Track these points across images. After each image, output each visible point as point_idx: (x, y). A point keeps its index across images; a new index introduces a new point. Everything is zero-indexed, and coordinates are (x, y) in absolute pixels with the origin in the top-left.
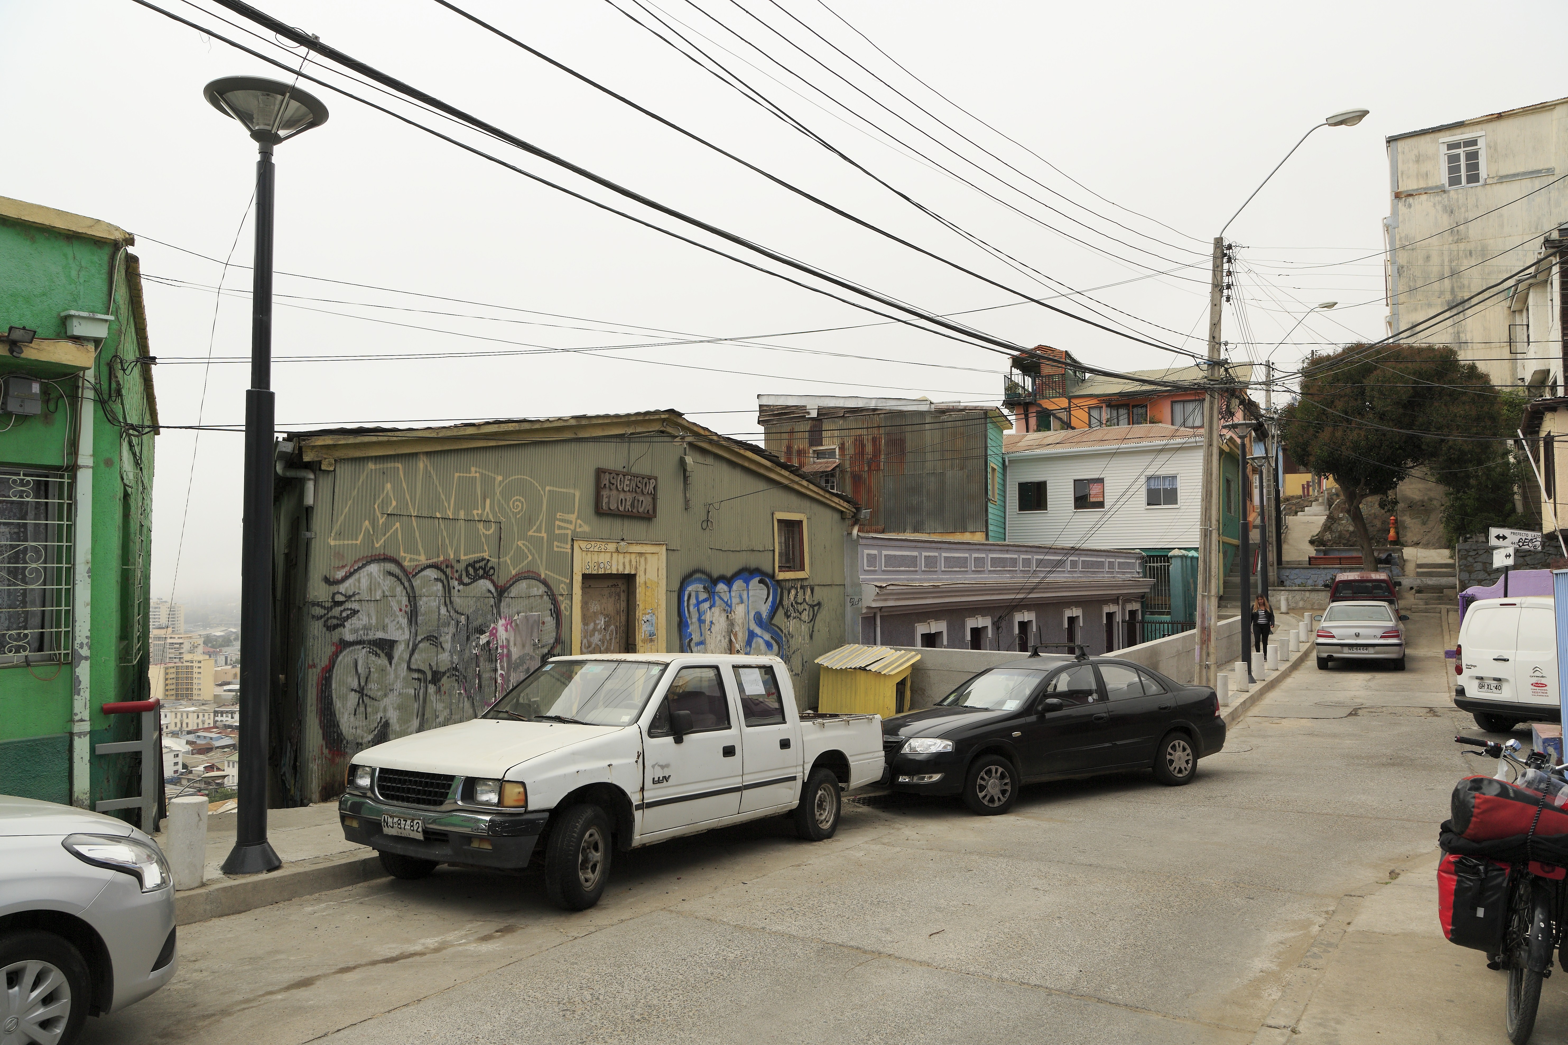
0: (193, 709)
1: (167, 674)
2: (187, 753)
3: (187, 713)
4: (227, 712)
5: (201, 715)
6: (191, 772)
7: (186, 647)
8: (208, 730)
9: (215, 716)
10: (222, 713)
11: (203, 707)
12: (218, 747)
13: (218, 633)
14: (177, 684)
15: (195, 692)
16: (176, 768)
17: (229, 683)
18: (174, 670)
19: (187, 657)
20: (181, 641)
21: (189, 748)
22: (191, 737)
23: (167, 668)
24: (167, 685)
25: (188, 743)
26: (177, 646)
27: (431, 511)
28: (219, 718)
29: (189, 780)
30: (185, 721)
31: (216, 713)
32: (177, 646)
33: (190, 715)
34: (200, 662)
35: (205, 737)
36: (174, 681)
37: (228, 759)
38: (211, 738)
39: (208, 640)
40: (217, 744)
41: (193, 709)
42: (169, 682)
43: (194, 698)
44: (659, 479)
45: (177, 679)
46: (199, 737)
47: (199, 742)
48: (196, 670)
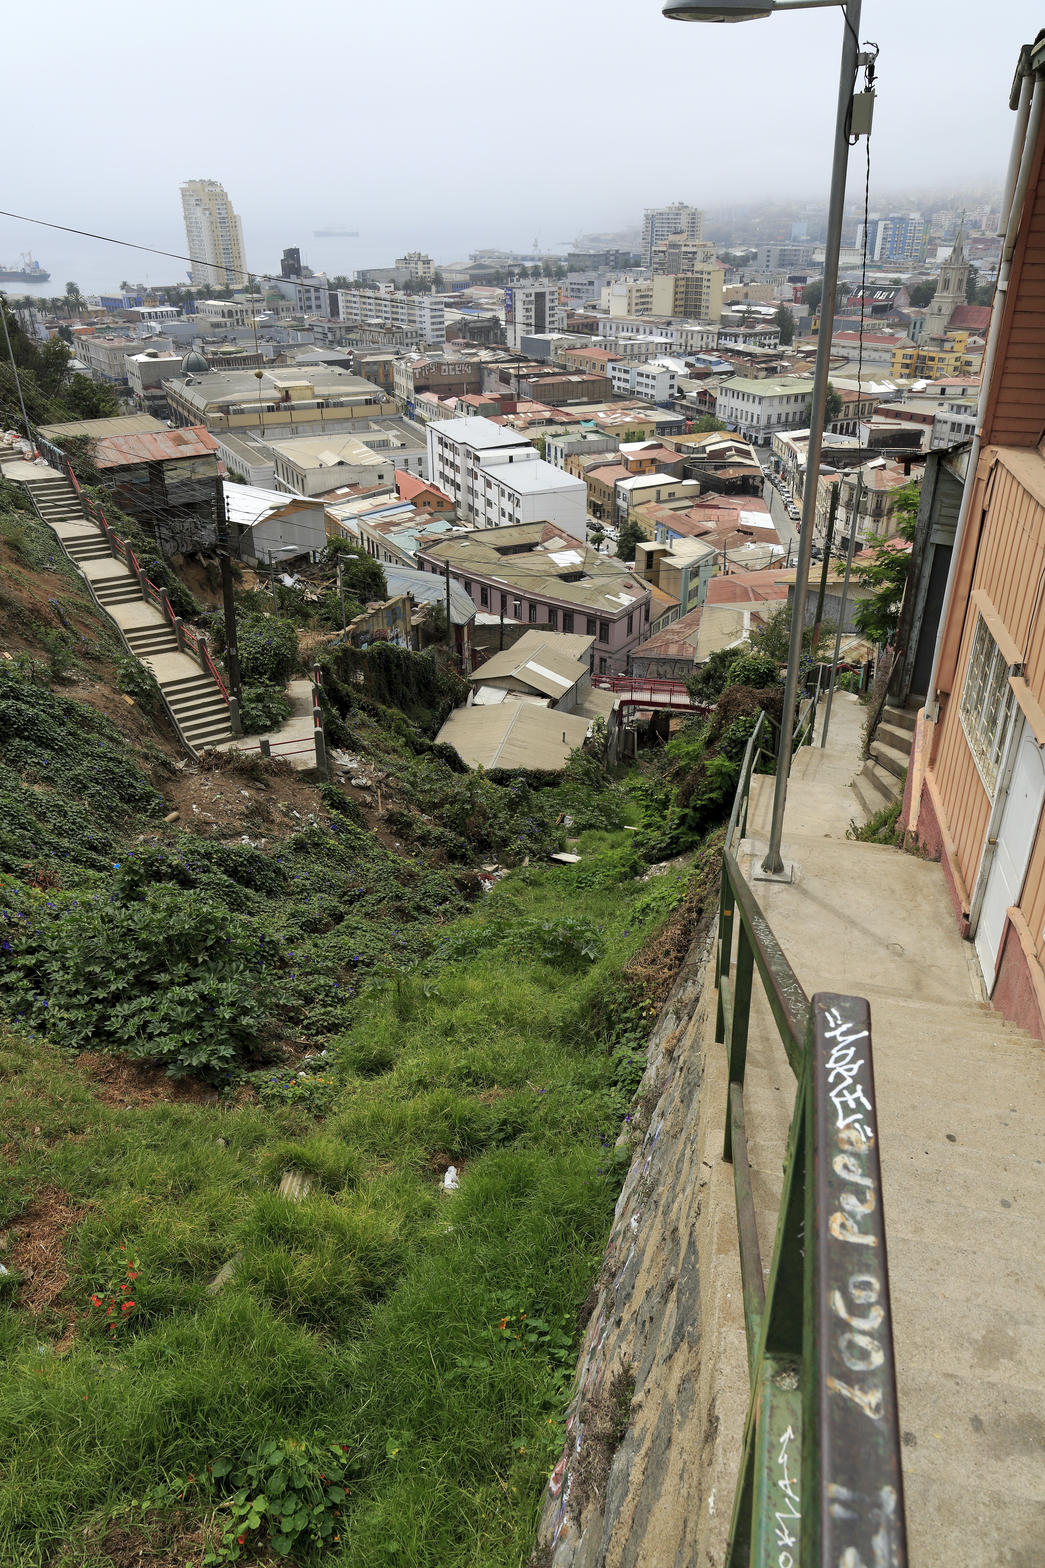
0: (698, 328)
1: (676, 286)
2: (685, 376)
3: (693, 332)
4: (731, 335)
5: (705, 336)
6: (684, 397)
7: (700, 256)
8: (709, 351)
9: (719, 339)
10: (726, 335)
11: (708, 328)
12: (716, 373)
13: (739, 253)
14: (686, 300)
15: (703, 310)
16: (671, 391)
17: (737, 303)
18: (683, 283)
19: (698, 266)
20: (694, 249)
21: (687, 371)
22: (691, 359)
23: (677, 280)
24: (676, 300)
25: (688, 365)
26: (690, 256)
27: (943, 520)
28: (722, 342)
29: (682, 406)
30: (690, 342)
31: (720, 335)
32: (690, 256)
33: (695, 336)
34: (709, 273)
35: (704, 360)
36: (683, 296)
37: (724, 385)
38: (710, 362)
39: (725, 259)
40: (716, 369)
41: (698, 328)
42: (679, 296)
43: (702, 317)
44: (859, 752)
45: (687, 293)
46: (698, 359)
47: (698, 365)
48: (705, 283)
